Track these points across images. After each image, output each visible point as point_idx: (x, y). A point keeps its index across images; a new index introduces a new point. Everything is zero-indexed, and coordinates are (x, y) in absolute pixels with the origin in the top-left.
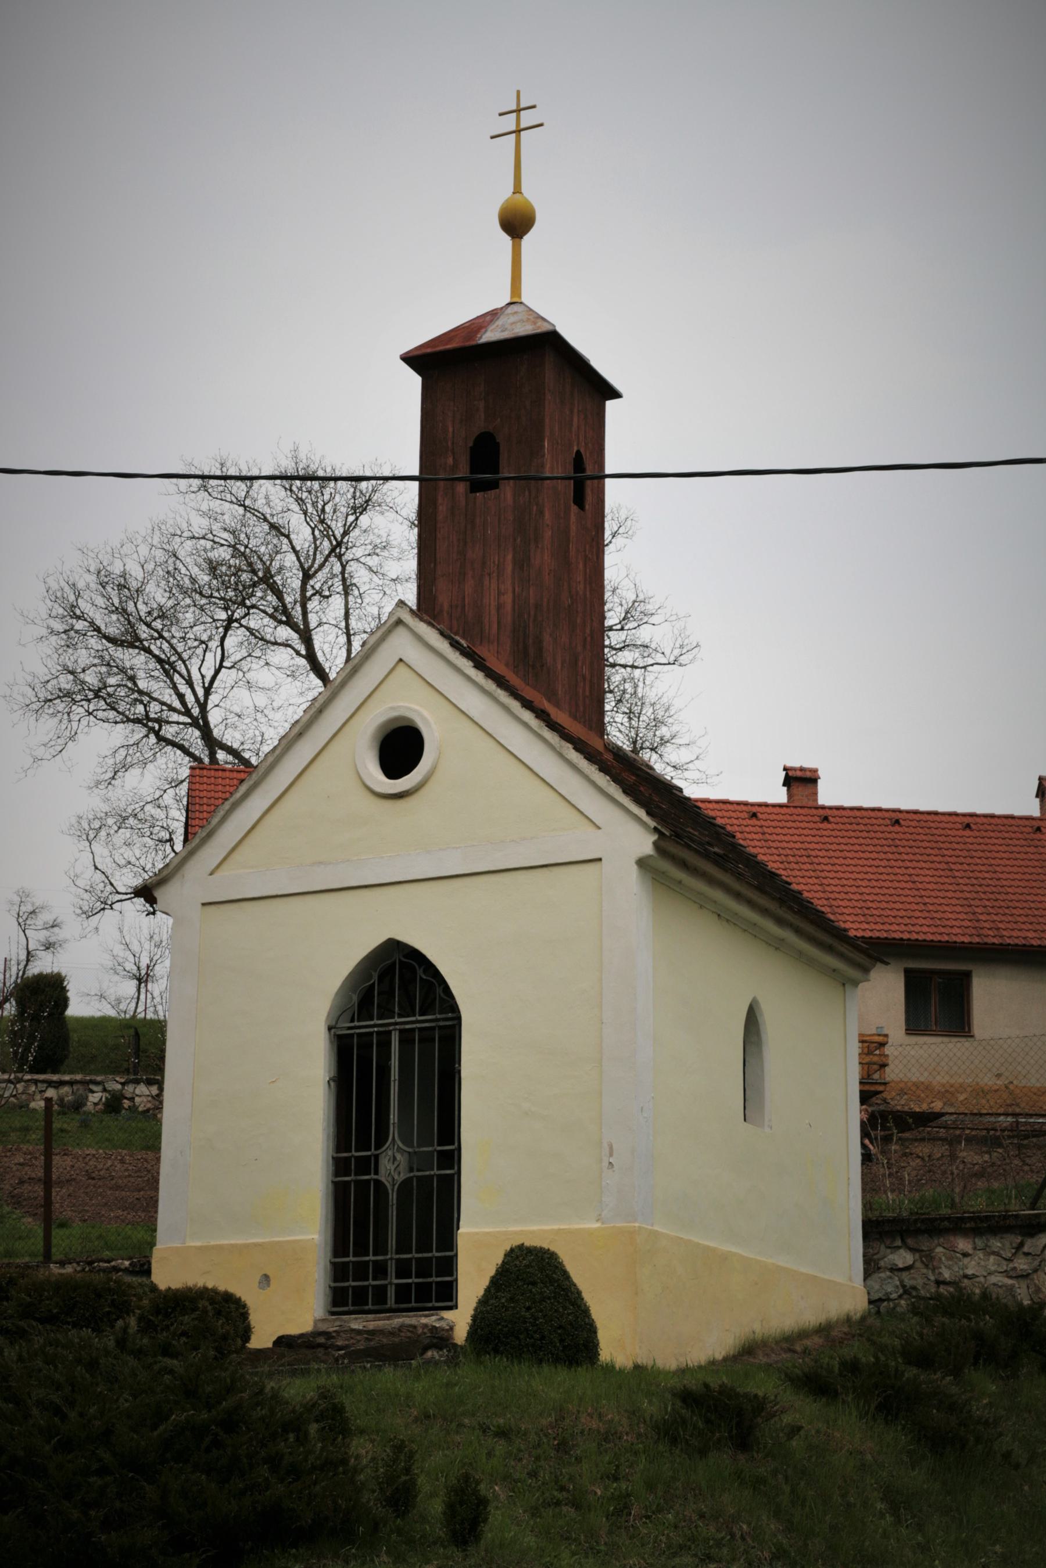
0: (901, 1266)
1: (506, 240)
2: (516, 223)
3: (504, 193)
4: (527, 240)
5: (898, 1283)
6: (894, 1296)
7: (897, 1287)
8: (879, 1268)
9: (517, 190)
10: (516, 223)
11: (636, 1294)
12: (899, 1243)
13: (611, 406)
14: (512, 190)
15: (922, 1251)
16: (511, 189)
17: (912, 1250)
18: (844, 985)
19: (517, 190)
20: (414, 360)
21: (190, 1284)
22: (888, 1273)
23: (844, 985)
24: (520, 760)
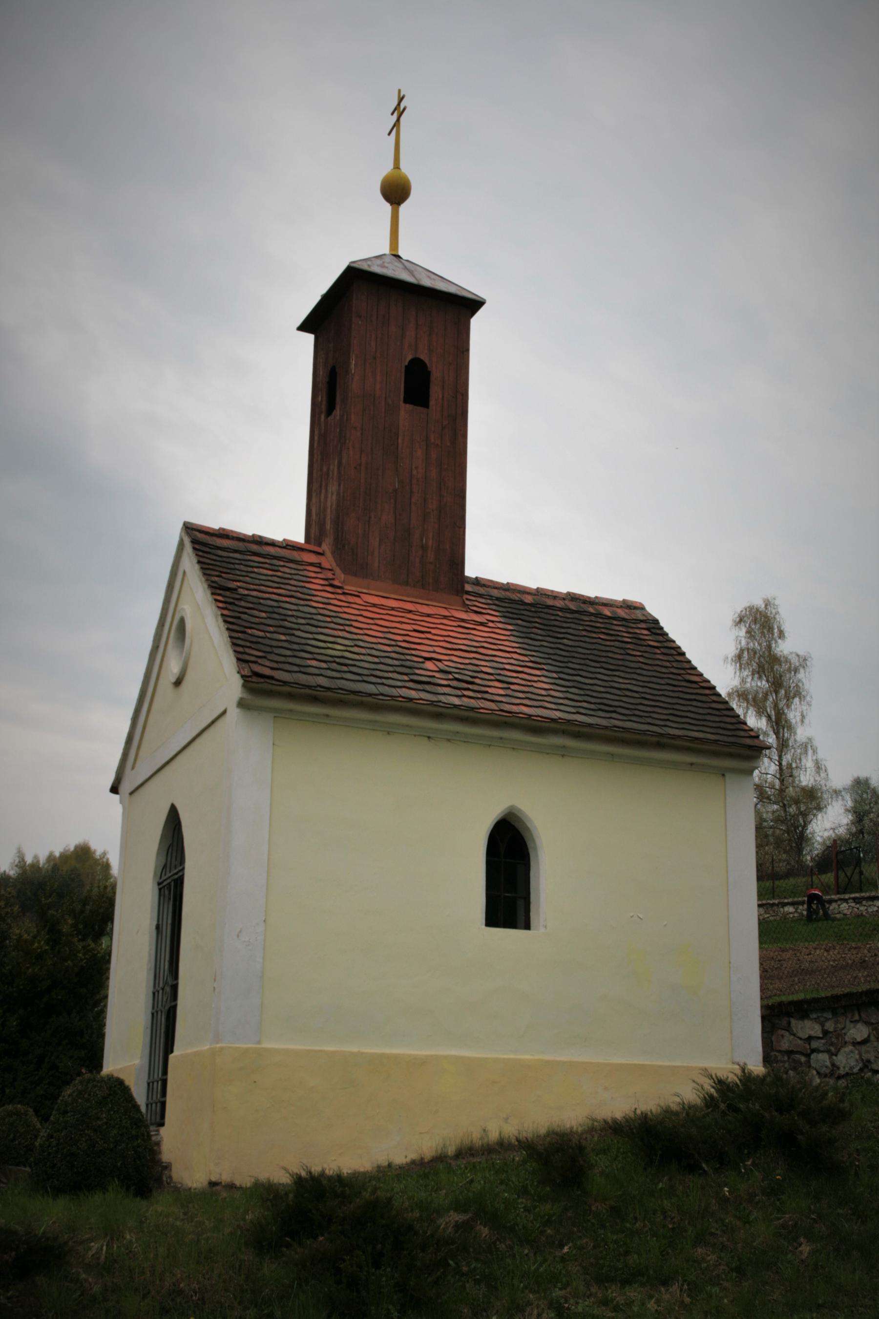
0: (859, 1040)
1: (387, 207)
2: (396, 192)
3: (387, 168)
4: (403, 208)
5: (857, 1057)
6: (856, 1070)
7: (857, 1060)
8: (846, 1043)
9: (397, 166)
10: (396, 192)
11: (215, 980)
12: (857, 1017)
13: (477, 323)
14: (392, 167)
15: (872, 1024)
16: (391, 166)
17: (867, 1023)
18: (723, 775)
19: (397, 166)
20: (305, 327)
21: (316, 1169)
22: (851, 1047)
23: (723, 775)
24: (213, 722)
